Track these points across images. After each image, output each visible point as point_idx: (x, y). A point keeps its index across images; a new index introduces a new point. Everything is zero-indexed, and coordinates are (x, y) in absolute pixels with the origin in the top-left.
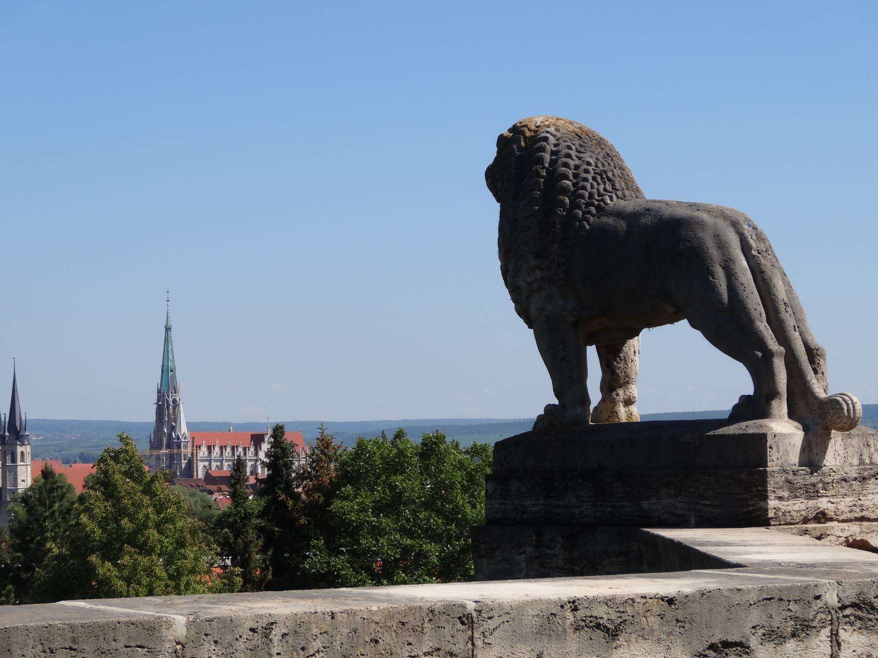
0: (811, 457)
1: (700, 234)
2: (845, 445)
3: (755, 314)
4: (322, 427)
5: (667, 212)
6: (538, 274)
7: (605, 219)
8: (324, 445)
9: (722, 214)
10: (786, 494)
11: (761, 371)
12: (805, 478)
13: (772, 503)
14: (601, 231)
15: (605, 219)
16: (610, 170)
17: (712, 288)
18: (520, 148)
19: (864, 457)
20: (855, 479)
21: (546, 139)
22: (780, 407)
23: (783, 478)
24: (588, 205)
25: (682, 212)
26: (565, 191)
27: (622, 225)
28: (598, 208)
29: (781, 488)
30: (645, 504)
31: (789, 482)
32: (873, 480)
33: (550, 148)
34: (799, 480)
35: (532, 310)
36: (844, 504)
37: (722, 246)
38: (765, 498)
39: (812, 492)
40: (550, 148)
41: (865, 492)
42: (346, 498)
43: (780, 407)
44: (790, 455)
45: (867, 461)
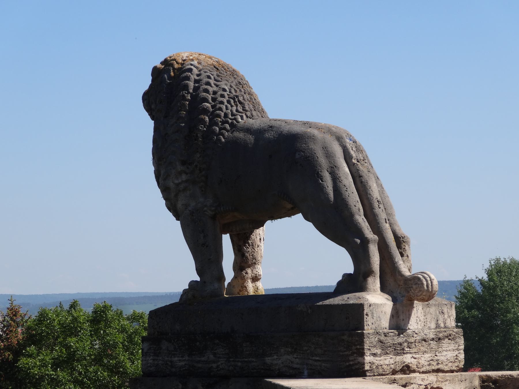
0: (399, 322)
1: (312, 146)
3: (354, 210)
4: (11, 299)
5: (286, 129)
6: (184, 177)
7: (237, 134)
8: (13, 312)
9: (329, 130)
10: (379, 351)
11: (359, 255)
12: (394, 339)
13: (368, 359)
14: (234, 143)
15: (237, 134)
16: (242, 96)
17: (321, 189)
18: (170, 77)
19: (439, 322)
20: (433, 339)
21: (190, 70)
22: (374, 282)
23: (376, 339)
24: (223, 122)
25: (297, 129)
26: (205, 111)
27: (250, 139)
28: (232, 125)
29: (375, 346)
30: (268, 360)
31: (381, 342)
32: (447, 340)
33: (193, 77)
34: (389, 341)
35: (179, 205)
36: (424, 359)
37: (329, 155)
38: (363, 354)
39: (399, 350)
40: (193, 77)
41: (440, 349)
42: (30, 356)
43: (374, 282)
44: (382, 321)
45: (442, 325)
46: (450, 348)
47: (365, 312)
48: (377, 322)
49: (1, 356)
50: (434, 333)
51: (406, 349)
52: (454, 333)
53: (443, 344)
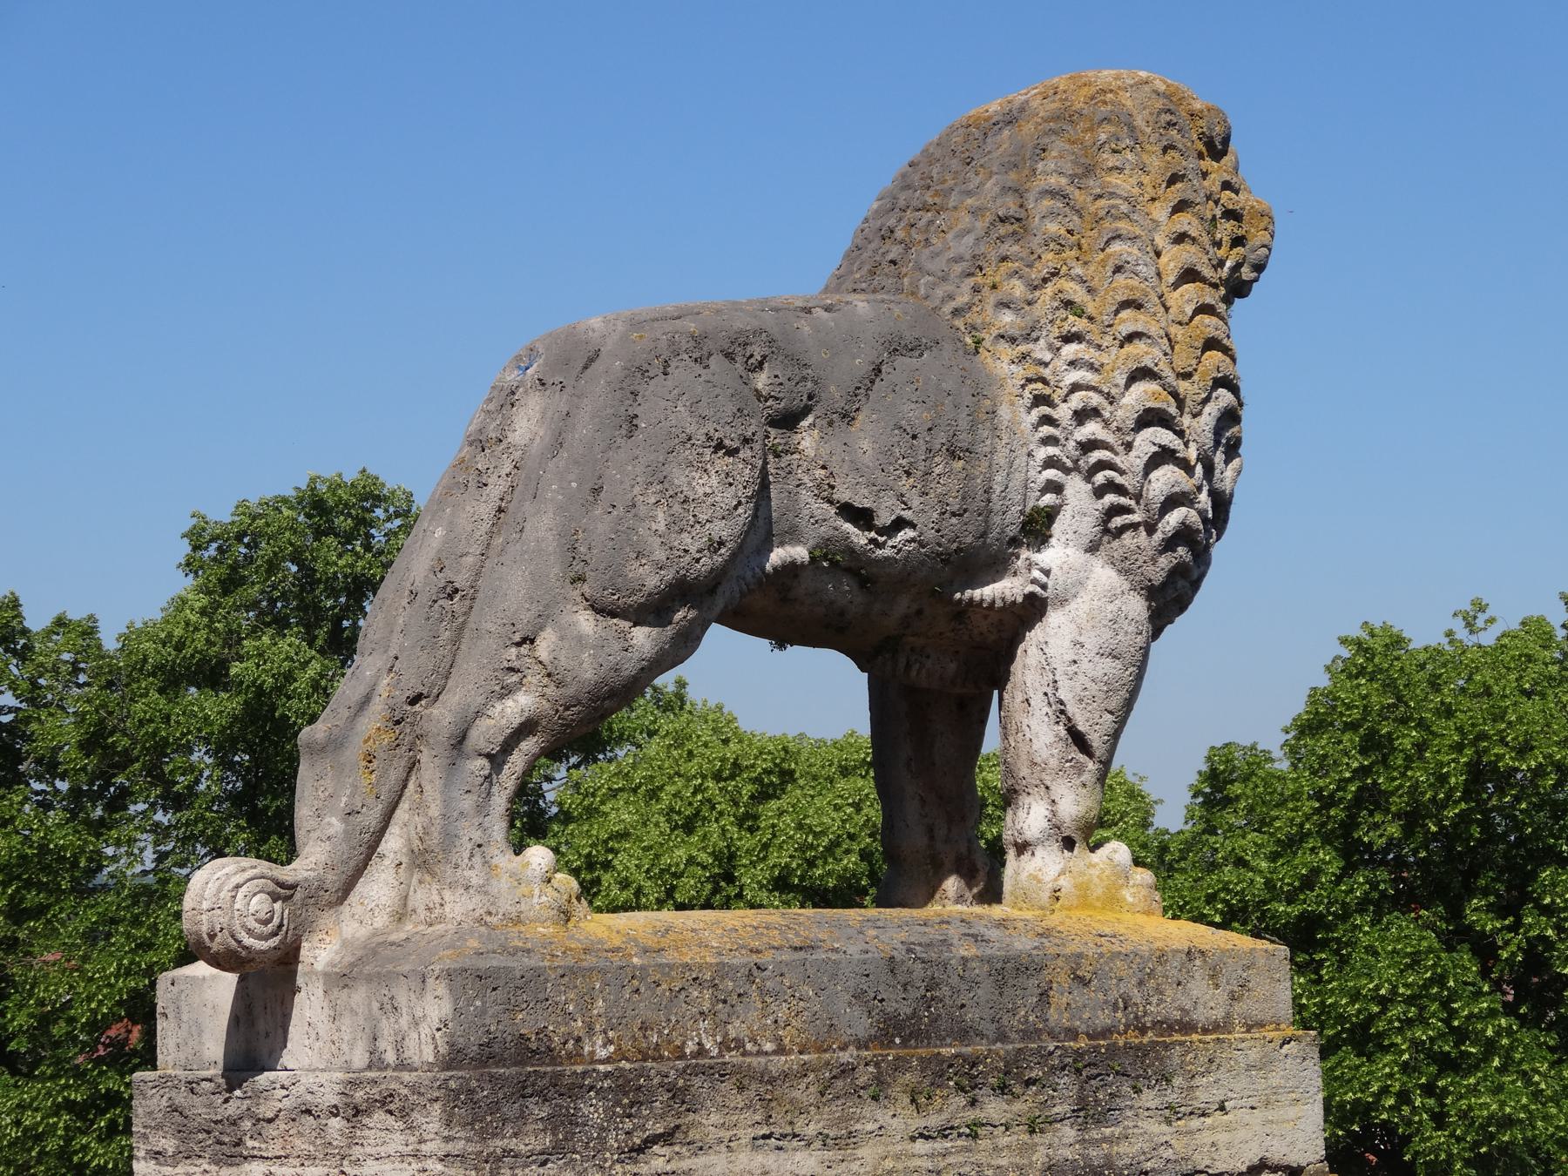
2: (334, 1008)
3: (1216, 413)
10: (169, 1144)
19: (382, 1044)
20: (334, 1112)
23: (164, 1102)
29: (159, 1127)
31: (174, 1109)
32: (379, 1116)
41: (357, 1152)
44: (206, 1036)
45: (390, 1057)
46: (391, 1149)
47: (159, 1009)
48: (191, 1043)
49: (1560, 1016)
50: (337, 1088)
51: (250, 1143)
52: (405, 1091)
53: (367, 1133)
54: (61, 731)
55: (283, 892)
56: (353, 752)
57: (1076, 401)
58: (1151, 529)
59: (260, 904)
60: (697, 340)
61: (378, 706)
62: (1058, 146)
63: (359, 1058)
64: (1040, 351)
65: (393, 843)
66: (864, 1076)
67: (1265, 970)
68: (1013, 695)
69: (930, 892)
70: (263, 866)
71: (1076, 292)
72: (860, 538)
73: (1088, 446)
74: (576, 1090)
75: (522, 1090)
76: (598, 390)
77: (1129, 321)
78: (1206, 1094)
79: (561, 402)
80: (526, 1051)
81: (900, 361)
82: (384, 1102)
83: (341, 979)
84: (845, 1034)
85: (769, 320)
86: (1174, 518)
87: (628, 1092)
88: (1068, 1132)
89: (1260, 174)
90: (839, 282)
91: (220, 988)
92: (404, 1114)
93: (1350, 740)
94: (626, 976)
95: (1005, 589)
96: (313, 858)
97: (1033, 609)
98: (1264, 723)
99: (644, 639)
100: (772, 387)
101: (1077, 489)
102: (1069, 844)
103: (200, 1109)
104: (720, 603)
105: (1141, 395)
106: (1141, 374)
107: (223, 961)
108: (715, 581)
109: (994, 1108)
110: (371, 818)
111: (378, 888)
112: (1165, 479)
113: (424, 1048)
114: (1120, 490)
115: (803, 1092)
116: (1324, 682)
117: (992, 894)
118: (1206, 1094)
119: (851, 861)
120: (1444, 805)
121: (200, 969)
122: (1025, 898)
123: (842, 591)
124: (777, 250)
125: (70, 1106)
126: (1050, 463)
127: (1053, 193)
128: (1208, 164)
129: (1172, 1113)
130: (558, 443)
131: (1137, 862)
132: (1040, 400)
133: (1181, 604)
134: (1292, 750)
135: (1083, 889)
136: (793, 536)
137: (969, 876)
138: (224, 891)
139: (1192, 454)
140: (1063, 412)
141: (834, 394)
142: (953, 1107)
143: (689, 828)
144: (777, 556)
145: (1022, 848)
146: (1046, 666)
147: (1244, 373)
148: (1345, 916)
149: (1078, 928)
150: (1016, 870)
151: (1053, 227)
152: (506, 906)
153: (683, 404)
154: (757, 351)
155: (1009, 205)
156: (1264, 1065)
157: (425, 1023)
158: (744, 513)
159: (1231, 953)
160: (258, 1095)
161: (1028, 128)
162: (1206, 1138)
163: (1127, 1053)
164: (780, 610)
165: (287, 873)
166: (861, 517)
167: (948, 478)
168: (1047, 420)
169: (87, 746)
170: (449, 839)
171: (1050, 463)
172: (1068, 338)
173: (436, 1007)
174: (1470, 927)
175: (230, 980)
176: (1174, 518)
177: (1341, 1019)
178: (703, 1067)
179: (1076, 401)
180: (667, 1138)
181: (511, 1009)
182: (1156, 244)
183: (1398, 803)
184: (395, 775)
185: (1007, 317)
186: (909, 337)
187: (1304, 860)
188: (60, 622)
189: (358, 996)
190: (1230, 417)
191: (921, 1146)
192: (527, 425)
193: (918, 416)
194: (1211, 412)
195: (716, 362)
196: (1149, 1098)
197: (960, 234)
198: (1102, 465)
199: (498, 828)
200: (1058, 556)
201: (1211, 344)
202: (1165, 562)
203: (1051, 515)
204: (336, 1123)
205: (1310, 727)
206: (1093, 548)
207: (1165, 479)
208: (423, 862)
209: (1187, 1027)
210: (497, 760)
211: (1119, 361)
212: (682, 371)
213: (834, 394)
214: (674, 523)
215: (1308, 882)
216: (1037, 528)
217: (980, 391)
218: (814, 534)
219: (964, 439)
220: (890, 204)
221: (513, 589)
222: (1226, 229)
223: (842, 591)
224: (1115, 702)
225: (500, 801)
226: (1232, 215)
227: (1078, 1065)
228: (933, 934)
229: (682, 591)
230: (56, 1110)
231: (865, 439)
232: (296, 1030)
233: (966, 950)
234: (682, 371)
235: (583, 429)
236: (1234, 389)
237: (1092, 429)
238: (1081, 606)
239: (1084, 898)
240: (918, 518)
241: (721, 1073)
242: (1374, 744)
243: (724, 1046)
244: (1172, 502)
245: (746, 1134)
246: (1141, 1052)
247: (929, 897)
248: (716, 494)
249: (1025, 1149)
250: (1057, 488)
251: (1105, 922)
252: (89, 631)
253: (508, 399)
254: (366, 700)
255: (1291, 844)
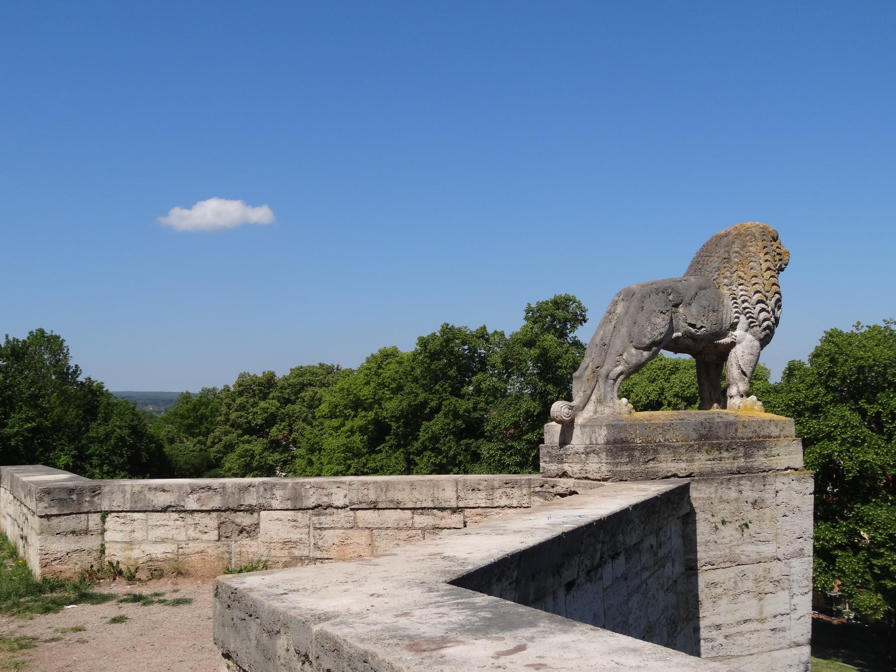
10: (548, 460)
20: (583, 453)
54: (496, 359)
55: (571, 408)
56: (585, 378)
57: (742, 298)
58: (760, 326)
59: (566, 410)
60: (656, 289)
61: (590, 369)
62: (737, 241)
63: (588, 442)
64: (734, 288)
65: (593, 397)
66: (696, 447)
67: (788, 424)
68: (728, 364)
69: (710, 407)
70: (567, 403)
71: (742, 274)
72: (693, 330)
73: (745, 308)
74: (633, 449)
75: (622, 449)
76: (635, 302)
77: (754, 280)
78: (774, 452)
79: (627, 304)
80: (623, 441)
81: (702, 292)
82: (593, 452)
83: (583, 426)
84: (691, 438)
85: (672, 284)
86: (765, 324)
87: (644, 450)
88: (742, 460)
89: (786, 243)
90: (688, 273)
91: (559, 427)
92: (598, 454)
93: (827, 359)
94: (643, 426)
95: (727, 340)
96: (576, 402)
97: (733, 344)
98: (803, 354)
99: (646, 354)
100: (672, 297)
101: (742, 318)
102: (742, 396)
103: (554, 452)
104: (662, 345)
105: (757, 297)
106: (757, 292)
107: (558, 422)
108: (661, 341)
109: (725, 454)
110: (589, 392)
111: (590, 407)
112: (763, 315)
113: (601, 440)
114: (753, 318)
115: (682, 450)
116: (819, 344)
117: (724, 407)
118: (774, 452)
119: (693, 390)
120: (851, 376)
121: (554, 423)
122: (732, 408)
123: (689, 342)
124: (672, 266)
125: (501, 449)
126: (736, 312)
127: (736, 252)
128: (773, 243)
129: (766, 456)
130: (627, 313)
131: (758, 400)
132: (734, 298)
133: (768, 343)
134: (811, 361)
135: (745, 406)
136: (678, 330)
137: (719, 402)
138: (559, 408)
139: (770, 309)
140: (739, 301)
141: (687, 299)
142: (716, 454)
143: (653, 382)
144: (675, 335)
145: (731, 397)
146: (736, 357)
147: (782, 290)
148: (826, 405)
149: (744, 415)
150: (730, 402)
151: (736, 260)
152: (617, 411)
153: (654, 303)
154: (669, 291)
155: (726, 255)
156: (788, 446)
157: (602, 435)
158: (667, 326)
159: (781, 420)
160: (566, 450)
161: (730, 237)
162: (774, 462)
163: (756, 442)
164: (675, 346)
165: (572, 404)
166: (693, 326)
167: (713, 317)
168: (735, 303)
169: (502, 363)
170: (605, 397)
171: (736, 312)
172: (740, 285)
173: (604, 432)
174: (861, 407)
175: (560, 426)
176: (765, 324)
177: (824, 432)
178: (660, 445)
179: (742, 298)
180: (653, 460)
181: (619, 432)
182: (761, 262)
183: (839, 375)
184: (594, 383)
185: (726, 280)
186: (703, 286)
187: (815, 391)
188: (496, 332)
189: (587, 429)
190: (779, 300)
191: (709, 462)
192: (620, 309)
193: (705, 303)
194: (774, 300)
195: (661, 294)
196: (761, 453)
197: (715, 262)
198: (748, 312)
199: (616, 395)
200: (738, 333)
201: (774, 284)
202: (763, 333)
203: (737, 324)
204: (583, 456)
205: (816, 355)
206: (746, 331)
207: (763, 315)
208: (600, 401)
209: (770, 437)
210: (615, 380)
211: (752, 289)
212: (653, 296)
213: (687, 299)
214: (653, 330)
215: (816, 396)
216: (734, 326)
217: (720, 298)
218: (683, 330)
219: (716, 308)
220: (699, 255)
221: (618, 344)
222: (777, 257)
223: (689, 342)
224: (752, 365)
225: (616, 389)
226: (778, 254)
227: (744, 445)
228: (711, 416)
229: (654, 344)
230: (498, 450)
231: (694, 309)
232: (574, 436)
233: (719, 420)
234: (653, 296)
235: (632, 310)
236: (780, 294)
237: (746, 304)
238: (744, 344)
239: (746, 408)
240: (706, 325)
241: (664, 446)
242: (833, 360)
243: (665, 440)
244: (765, 320)
245: (670, 459)
246: (759, 442)
247: (710, 408)
248: (661, 323)
249: (732, 463)
250: (738, 318)
251: (750, 413)
252: (502, 335)
253: (615, 303)
254: (587, 367)
255: (812, 385)
